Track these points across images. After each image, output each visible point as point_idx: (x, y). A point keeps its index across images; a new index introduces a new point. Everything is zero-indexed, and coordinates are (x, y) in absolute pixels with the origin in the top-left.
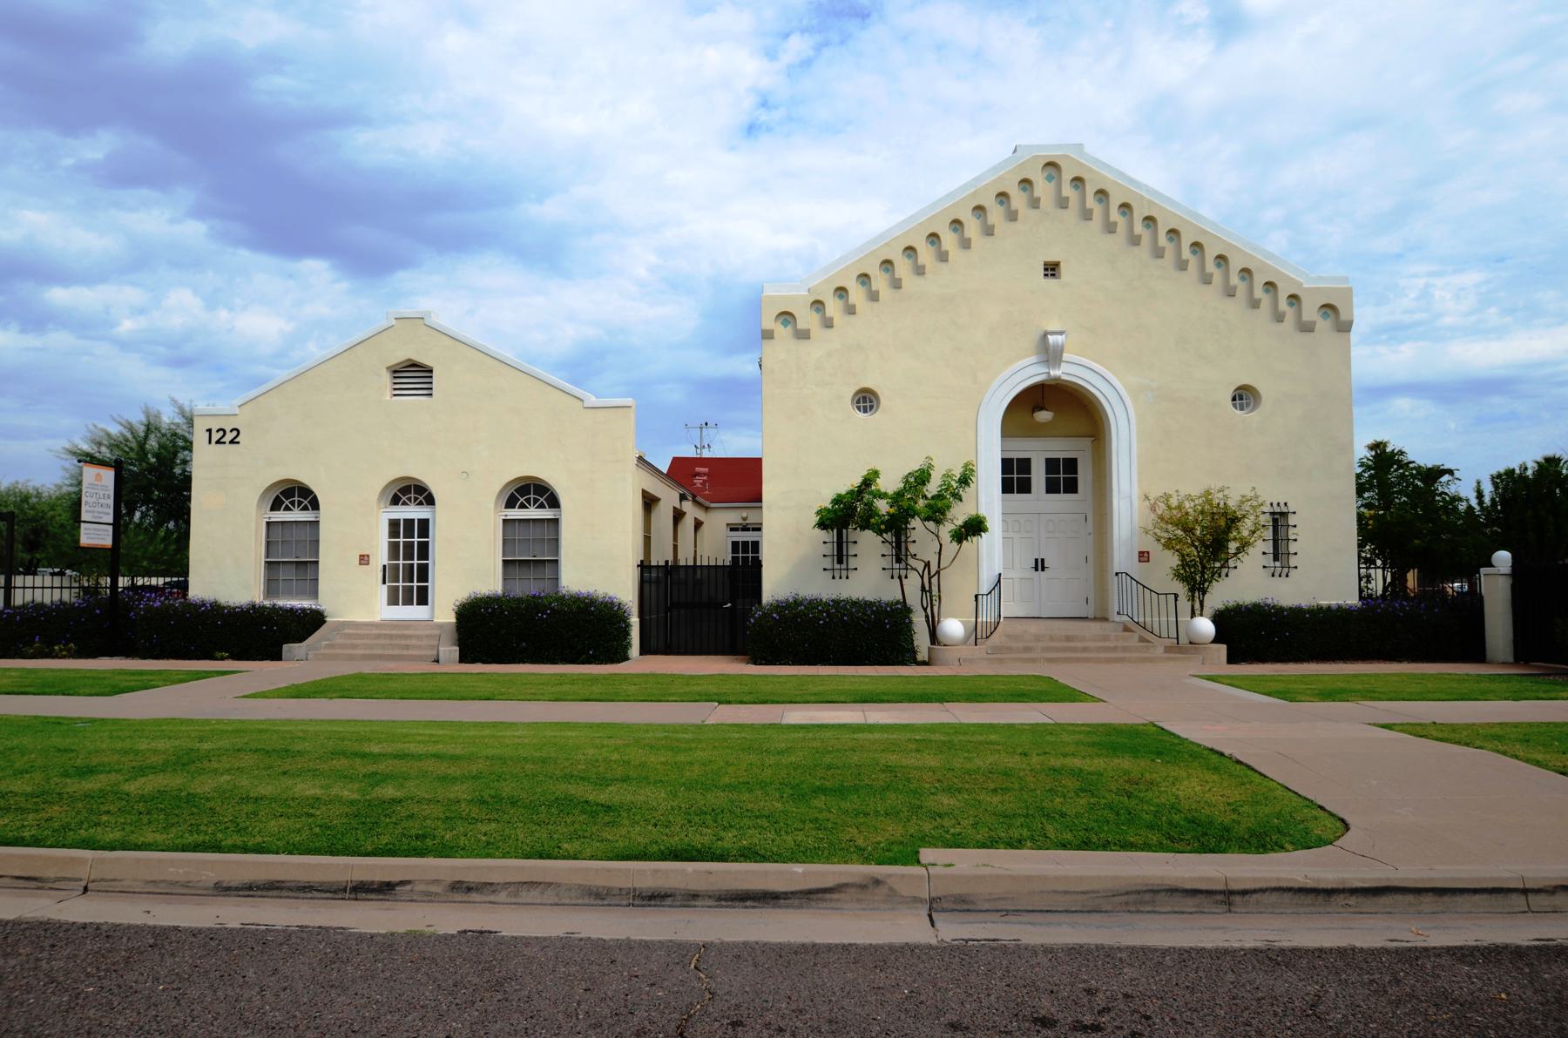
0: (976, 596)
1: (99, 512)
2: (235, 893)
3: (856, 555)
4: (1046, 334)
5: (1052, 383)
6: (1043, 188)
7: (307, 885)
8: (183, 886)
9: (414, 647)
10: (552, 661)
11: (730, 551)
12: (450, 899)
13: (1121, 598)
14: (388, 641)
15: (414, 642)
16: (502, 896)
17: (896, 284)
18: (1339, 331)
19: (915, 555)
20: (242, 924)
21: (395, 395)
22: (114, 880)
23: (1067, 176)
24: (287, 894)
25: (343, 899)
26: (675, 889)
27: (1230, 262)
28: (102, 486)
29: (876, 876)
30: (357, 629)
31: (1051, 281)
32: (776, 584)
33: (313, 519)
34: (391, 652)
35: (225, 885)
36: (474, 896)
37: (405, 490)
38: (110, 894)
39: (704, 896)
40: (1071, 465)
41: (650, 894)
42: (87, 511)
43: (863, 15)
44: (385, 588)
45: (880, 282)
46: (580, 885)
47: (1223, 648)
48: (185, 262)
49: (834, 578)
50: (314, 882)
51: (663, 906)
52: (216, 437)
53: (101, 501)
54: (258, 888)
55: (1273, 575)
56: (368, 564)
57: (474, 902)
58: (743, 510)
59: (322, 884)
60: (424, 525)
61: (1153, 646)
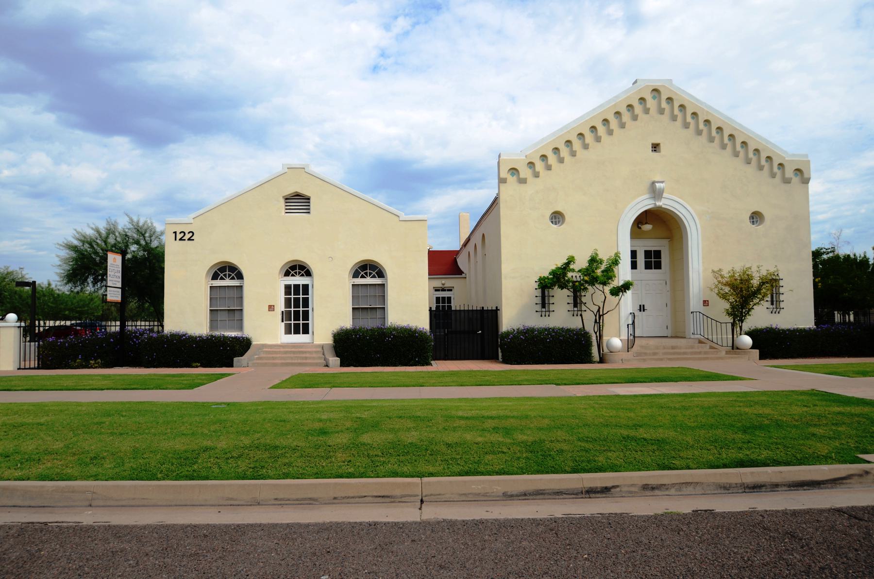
0: (628, 325)
1: (115, 281)
2: (517, 498)
3: (553, 304)
4: (653, 183)
5: (657, 210)
6: (651, 103)
7: (558, 491)
8: (484, 496)
9: (310, 358)
10: (394, 365)
11: (351, 305)
12: (643, 495)
13: (695, 323)
14: (292, 355)
15: (308, 355)
16: (673, 491)
17: (573, 154)
18: (803, 183)
19: (585, 303)
20: (750, 508)
21: (286, 213)
22: (439, 495)
23: (664, 97)
24: (549, 497)
25: (582, 498)
26: (766, 482)
27: (749, 145)
28: (116, 265)
29: (866, 470)
30: (271, 349)
31: (655, 154)
32: (509, 321)
33: (239, 285)
34: (296, 361)
35: (509, 494)
36: (657, 492)
37: (293, 268)
38: (438, 503)
39: (781, 485)
40: (658, 254)
41: (753, 486)
42: (110, 280)
43: (438, 8)
44: (283, 324)
45: (565, 152)
46: (714, 483)
47: (756, 352)
48: (42, 137)
49: (541, 316)
50: (562, 489)
51: (761, 492)
52: (179, 236)
53: (116, 274)
54: (530, 494)
55: (772, 313)
56: (274, 310)
57: (658, 496)
58: (443, 279)
59: (568, 490)
60: (306, 288)
61: (719, 351)
